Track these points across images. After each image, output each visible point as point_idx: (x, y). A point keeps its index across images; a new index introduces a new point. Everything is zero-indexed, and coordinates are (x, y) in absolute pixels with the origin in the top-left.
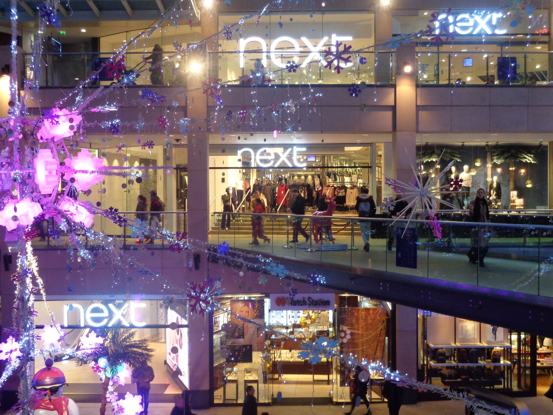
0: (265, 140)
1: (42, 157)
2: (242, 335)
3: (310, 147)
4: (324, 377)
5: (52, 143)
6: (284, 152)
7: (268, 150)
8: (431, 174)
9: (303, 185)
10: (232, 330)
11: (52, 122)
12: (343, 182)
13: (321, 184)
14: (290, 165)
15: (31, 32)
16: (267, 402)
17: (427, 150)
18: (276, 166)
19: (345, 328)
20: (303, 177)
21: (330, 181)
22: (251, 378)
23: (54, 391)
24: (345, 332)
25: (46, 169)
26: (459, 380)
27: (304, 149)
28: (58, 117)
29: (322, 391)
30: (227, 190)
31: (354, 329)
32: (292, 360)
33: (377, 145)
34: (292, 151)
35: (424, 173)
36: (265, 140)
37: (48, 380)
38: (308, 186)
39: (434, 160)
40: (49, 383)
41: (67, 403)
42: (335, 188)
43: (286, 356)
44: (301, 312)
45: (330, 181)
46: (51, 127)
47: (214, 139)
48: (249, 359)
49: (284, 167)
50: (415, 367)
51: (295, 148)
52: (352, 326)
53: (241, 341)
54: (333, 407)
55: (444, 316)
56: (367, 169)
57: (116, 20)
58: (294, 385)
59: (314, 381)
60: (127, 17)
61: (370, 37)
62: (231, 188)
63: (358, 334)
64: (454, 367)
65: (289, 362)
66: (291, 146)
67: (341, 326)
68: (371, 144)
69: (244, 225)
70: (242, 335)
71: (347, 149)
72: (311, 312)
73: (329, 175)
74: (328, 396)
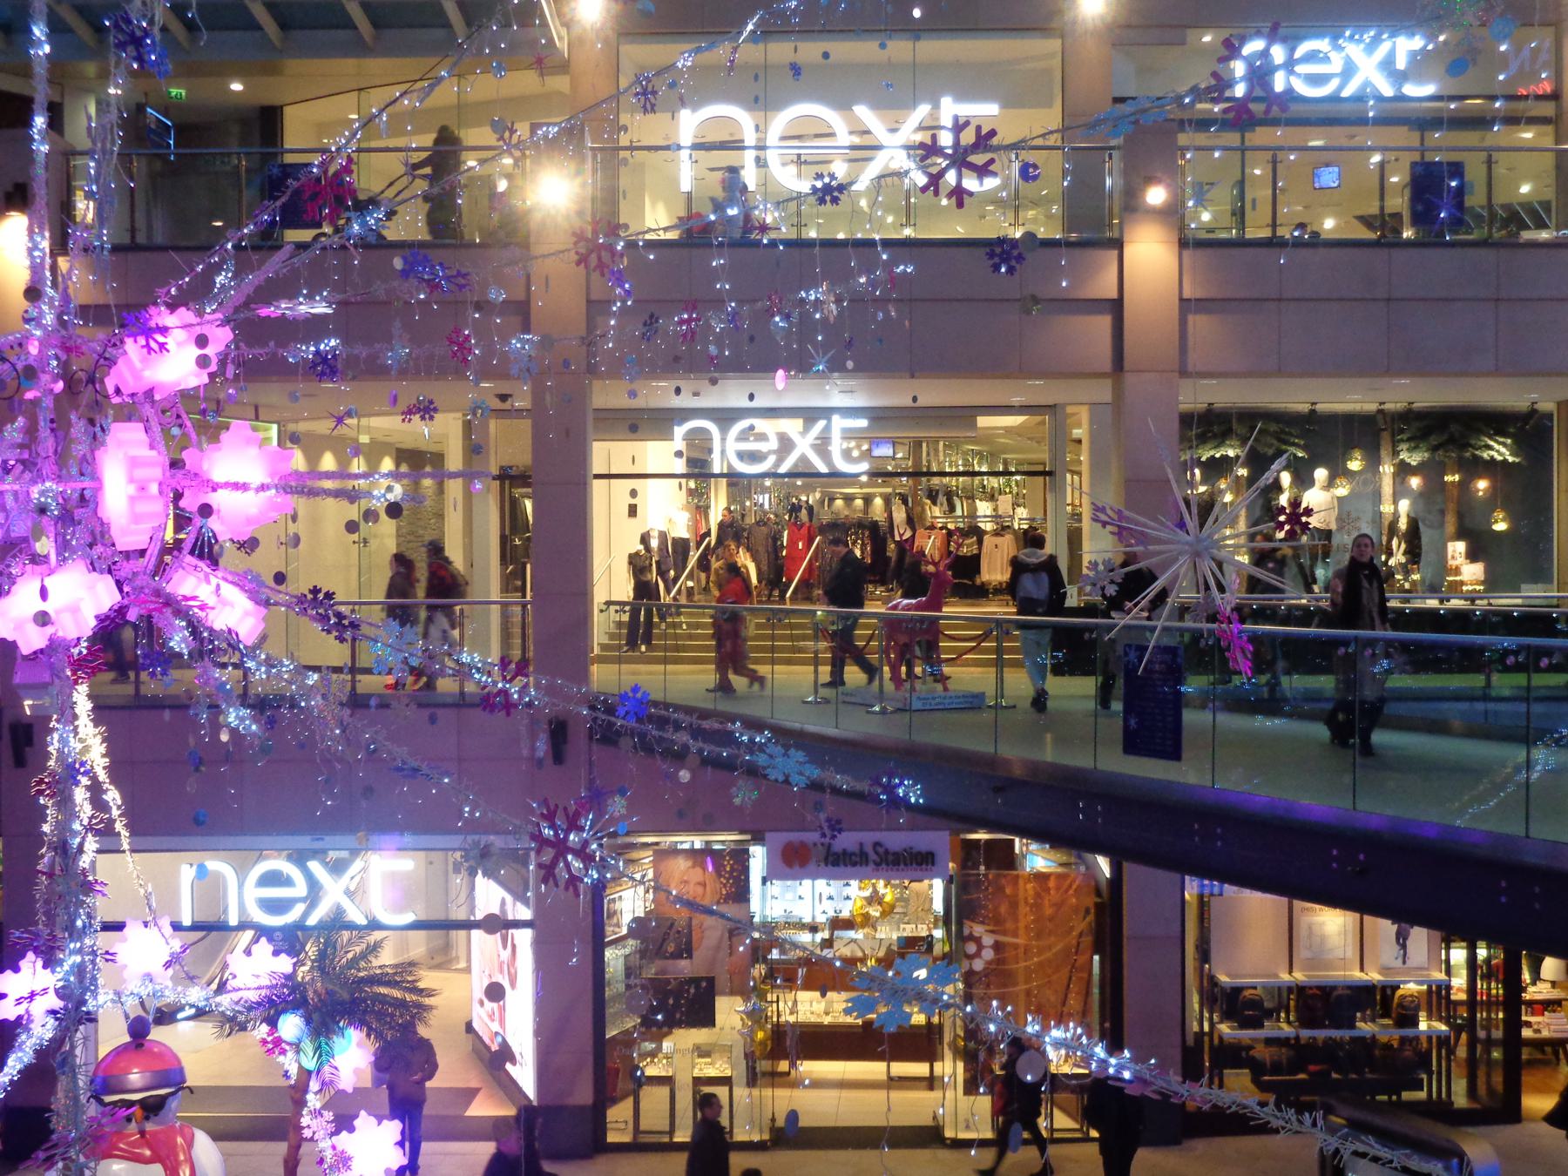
0: (751, 397)
1: (120, 444)
2: (686, 950)
3: (879, 416)
4: (920, 1069)
5: (146, 406)
6: (806, 429)
7: (761, 425)
8: (1222, 492)
9: (860, 525)
10: (658, 936)
11: (147, 346)
12: (973, 514)
13: (910, 521)
14: (823, 469)
15: (88, 91)
16: (756, 1138)
17: (1209, 425)
18: (783, 469)
19: (978, 930)
20: (859, 502)
21: (935, 512)
22: (712, 1072)
23: (153, 1108)
24: (978, 941)
25: (131, 480)
26: (1302, 1076)
27: (863, 423)
28: (164, 330)
29: (913, 1108)
30: (645, 539)
31: (1004, 933)
32: (827, 1020)
33: (1069, 410)
34: (827, 428)
35: (1202, 489)
36: (751, 397)
37: (135, 1078)
38: (874, 527)
39: (1231, 453)
40: (139, 1085)
41: (190, 1143)
42: (950, 533)
43: (810, 1007)
44: (854, 883)
45: (935, 512)
46: (143, 360)
47: (607, 395)
48: (706, 1018)
49: (804, 473)
50: (1177, 1039)
51: (836, 418)
52: (997, 925)
53: (684, 967)
54: (944, 1154)
55: (1258, 895)
56: (1041, 479)
57: (329, 56)
58: (833, 1090)
59: (891, 1079)
60: (361, 49)
61: (1049, 105)
62: (655, 534)
63: (1016, 947)
64: (1288, 1039)
65: (820, 1026)
66: (826, 412)
67: (967, 923)
68: (1051, 408)
69: (691, 637)
70: (686, 950)
71: (983, 421)
72: (881, 883)
73: (933, 496)
74: (929, 1122)
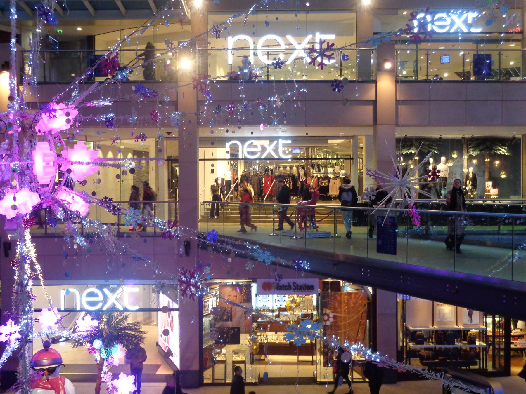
0: (252, 133)
1: (40, 149)
2: (230, 318)
3: (295, 139)
4: (309, 358)
5: (49, 136)
6: (270, 144)
7: (255, 142)
8: (410, 165)
9: (289, 176)
10: (221, 314)
11: (49, 116)
12: (326, 172)
13: (305, 175)
14: (276, 157)
15: (29, 30)
16: (254, 381)
17: (406, 142)
18: (263, 157)
19: (328, 311)
20: (288, 168)
21: (314, 172)
22: (239, 359)
23: (51, 371)
24: (328, 315)
25: (44, 161)
26: (437, 361)
27: (289, 142)
28: (55, 111)
29: (306, 371)
30: (216, 181)
31: (337, 313)
32: (277, 342)
33: (359, 137)
34: (278, 144)
35: (403, 164)
36: (252, 133)
37: (45, 361)
38: (293, 176)
39: (413, 152)
40: (47, 363)
41: (64, 383)
42: (319, 179)
43: (272, 338)
44: (287, 296)
45: (314, 172)
46: (48, 121)
47: (204, 132)
48: (237, 341)
49: (270, 159)
50: (395, 348)
51: (280, 140)
52: (334, 310)
53: (230, 324)
54: (317, 387)
56: (349, 160)
57: (110, 19)
58: (279, 365)
59: (299, 361)
60: (121, 16)
61: (352, 35)
62: (220, 179)
63: (341, 317)
64: (432, 348)
65: (275, 344)
66: (277, 138)
67: (324, 309)
68: (353, 137)
69: (232, 213)
70: (230, 318)
71: (330, 141)
72: (296, 296)
73: (313, 166)
74: (312, 376)
